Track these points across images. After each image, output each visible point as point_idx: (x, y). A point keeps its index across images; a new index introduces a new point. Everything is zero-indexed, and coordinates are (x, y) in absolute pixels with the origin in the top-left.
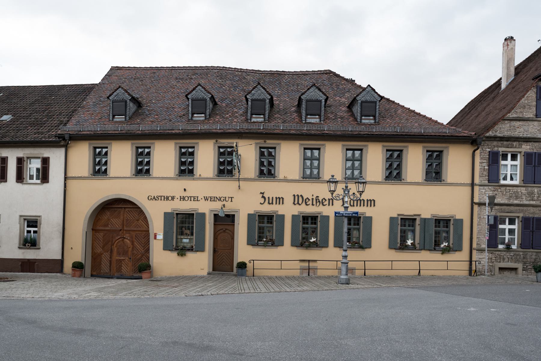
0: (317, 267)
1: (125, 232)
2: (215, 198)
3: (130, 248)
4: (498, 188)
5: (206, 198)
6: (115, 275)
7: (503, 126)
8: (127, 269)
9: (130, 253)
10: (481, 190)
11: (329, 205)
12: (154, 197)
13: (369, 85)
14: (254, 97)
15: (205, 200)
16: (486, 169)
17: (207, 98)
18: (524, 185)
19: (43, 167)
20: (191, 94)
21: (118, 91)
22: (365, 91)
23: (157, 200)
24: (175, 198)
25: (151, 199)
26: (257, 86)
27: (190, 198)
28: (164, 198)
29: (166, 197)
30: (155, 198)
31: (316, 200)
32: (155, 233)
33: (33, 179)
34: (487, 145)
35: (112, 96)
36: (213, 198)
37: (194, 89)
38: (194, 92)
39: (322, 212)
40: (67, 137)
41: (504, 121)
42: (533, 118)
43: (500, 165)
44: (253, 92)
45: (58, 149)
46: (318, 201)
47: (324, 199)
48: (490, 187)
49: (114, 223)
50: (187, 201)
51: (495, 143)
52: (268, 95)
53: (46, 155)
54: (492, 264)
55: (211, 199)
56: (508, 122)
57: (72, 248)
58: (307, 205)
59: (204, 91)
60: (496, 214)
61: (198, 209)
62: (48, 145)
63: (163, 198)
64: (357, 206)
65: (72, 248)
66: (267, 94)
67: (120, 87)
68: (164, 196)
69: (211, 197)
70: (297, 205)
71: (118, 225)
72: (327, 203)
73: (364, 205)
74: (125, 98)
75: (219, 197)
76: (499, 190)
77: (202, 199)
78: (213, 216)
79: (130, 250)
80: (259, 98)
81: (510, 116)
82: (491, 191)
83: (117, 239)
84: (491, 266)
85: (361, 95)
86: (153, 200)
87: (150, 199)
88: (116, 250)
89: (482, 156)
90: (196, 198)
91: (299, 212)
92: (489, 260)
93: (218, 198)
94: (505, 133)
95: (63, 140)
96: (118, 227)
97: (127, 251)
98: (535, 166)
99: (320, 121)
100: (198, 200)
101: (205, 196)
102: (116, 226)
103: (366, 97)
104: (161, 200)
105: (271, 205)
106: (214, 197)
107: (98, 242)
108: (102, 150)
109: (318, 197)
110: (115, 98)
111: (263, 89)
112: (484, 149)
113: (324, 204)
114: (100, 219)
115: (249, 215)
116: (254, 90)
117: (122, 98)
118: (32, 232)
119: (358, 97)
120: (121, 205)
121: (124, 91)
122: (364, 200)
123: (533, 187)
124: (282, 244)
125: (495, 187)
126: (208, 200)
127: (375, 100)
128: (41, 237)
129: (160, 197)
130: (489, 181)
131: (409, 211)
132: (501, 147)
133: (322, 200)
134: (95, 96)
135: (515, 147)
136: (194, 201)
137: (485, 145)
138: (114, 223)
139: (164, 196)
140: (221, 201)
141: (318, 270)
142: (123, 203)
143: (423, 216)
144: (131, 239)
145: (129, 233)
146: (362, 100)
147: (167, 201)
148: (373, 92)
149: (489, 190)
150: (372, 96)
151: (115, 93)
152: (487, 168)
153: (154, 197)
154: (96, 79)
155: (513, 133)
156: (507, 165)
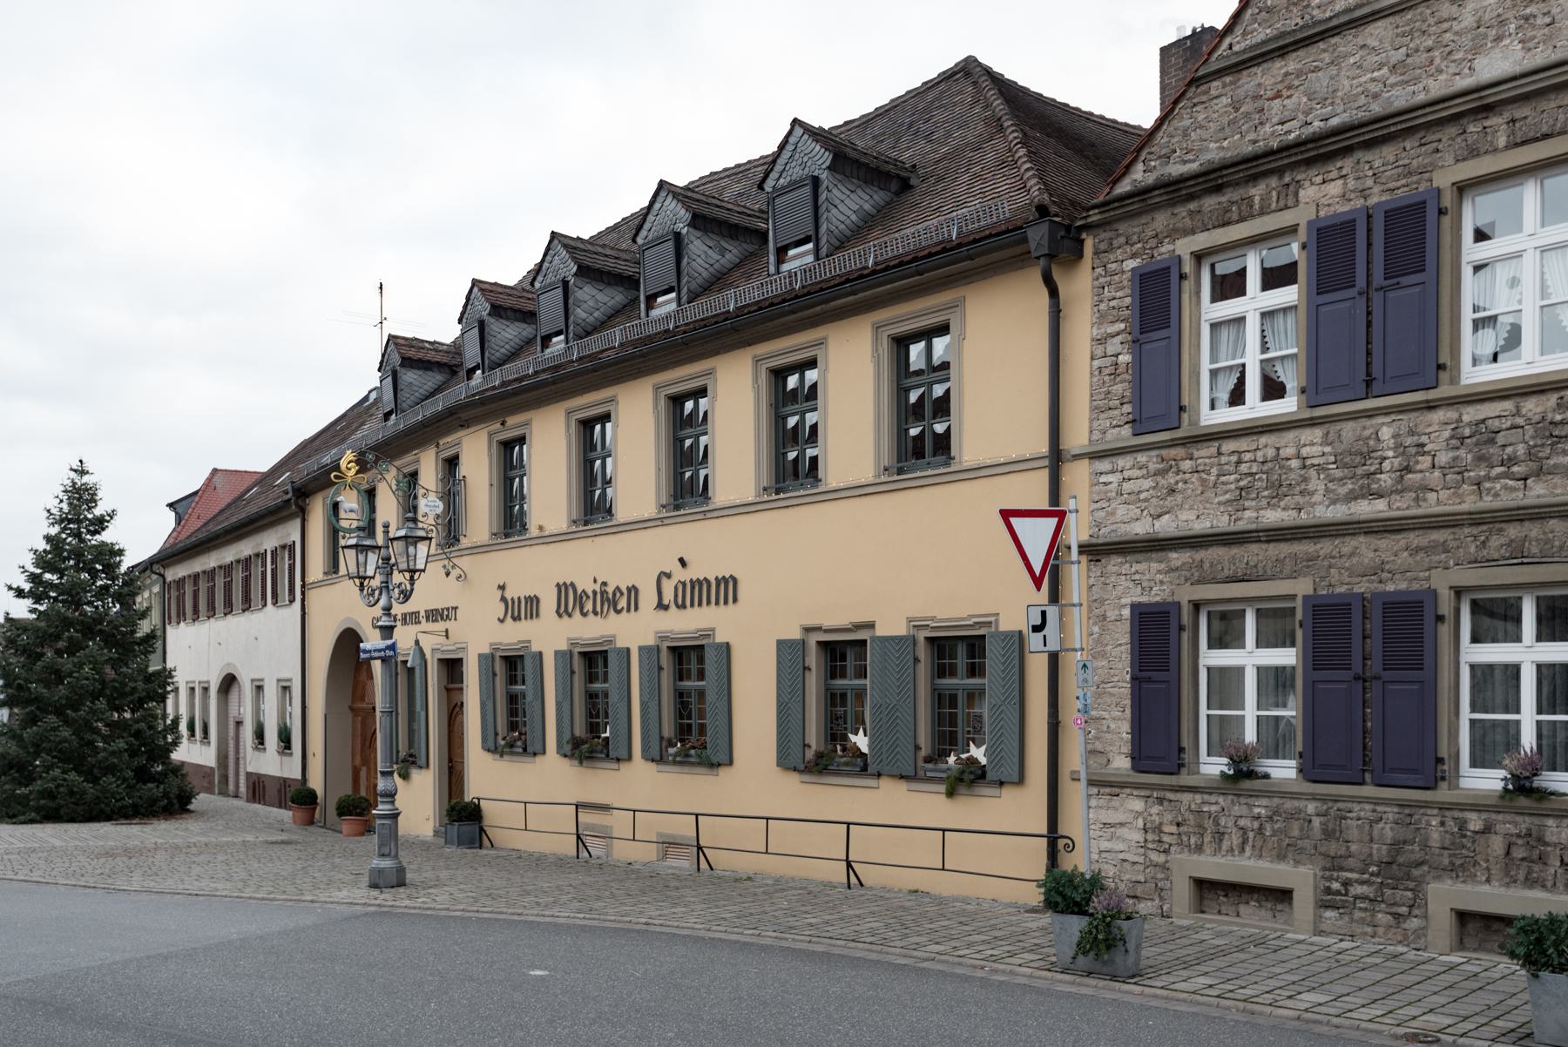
10: (1103, 479)
11: (628, 610)
48: (1142, 458)
51: (1161, 220)
61: (529, 642)
72: (623, 603)
76: (1187, 465)
89: (1103, 306)
92: (1150, 837)
112: (1114, 266)
125: (1164, 452)
155: (1252, 136)
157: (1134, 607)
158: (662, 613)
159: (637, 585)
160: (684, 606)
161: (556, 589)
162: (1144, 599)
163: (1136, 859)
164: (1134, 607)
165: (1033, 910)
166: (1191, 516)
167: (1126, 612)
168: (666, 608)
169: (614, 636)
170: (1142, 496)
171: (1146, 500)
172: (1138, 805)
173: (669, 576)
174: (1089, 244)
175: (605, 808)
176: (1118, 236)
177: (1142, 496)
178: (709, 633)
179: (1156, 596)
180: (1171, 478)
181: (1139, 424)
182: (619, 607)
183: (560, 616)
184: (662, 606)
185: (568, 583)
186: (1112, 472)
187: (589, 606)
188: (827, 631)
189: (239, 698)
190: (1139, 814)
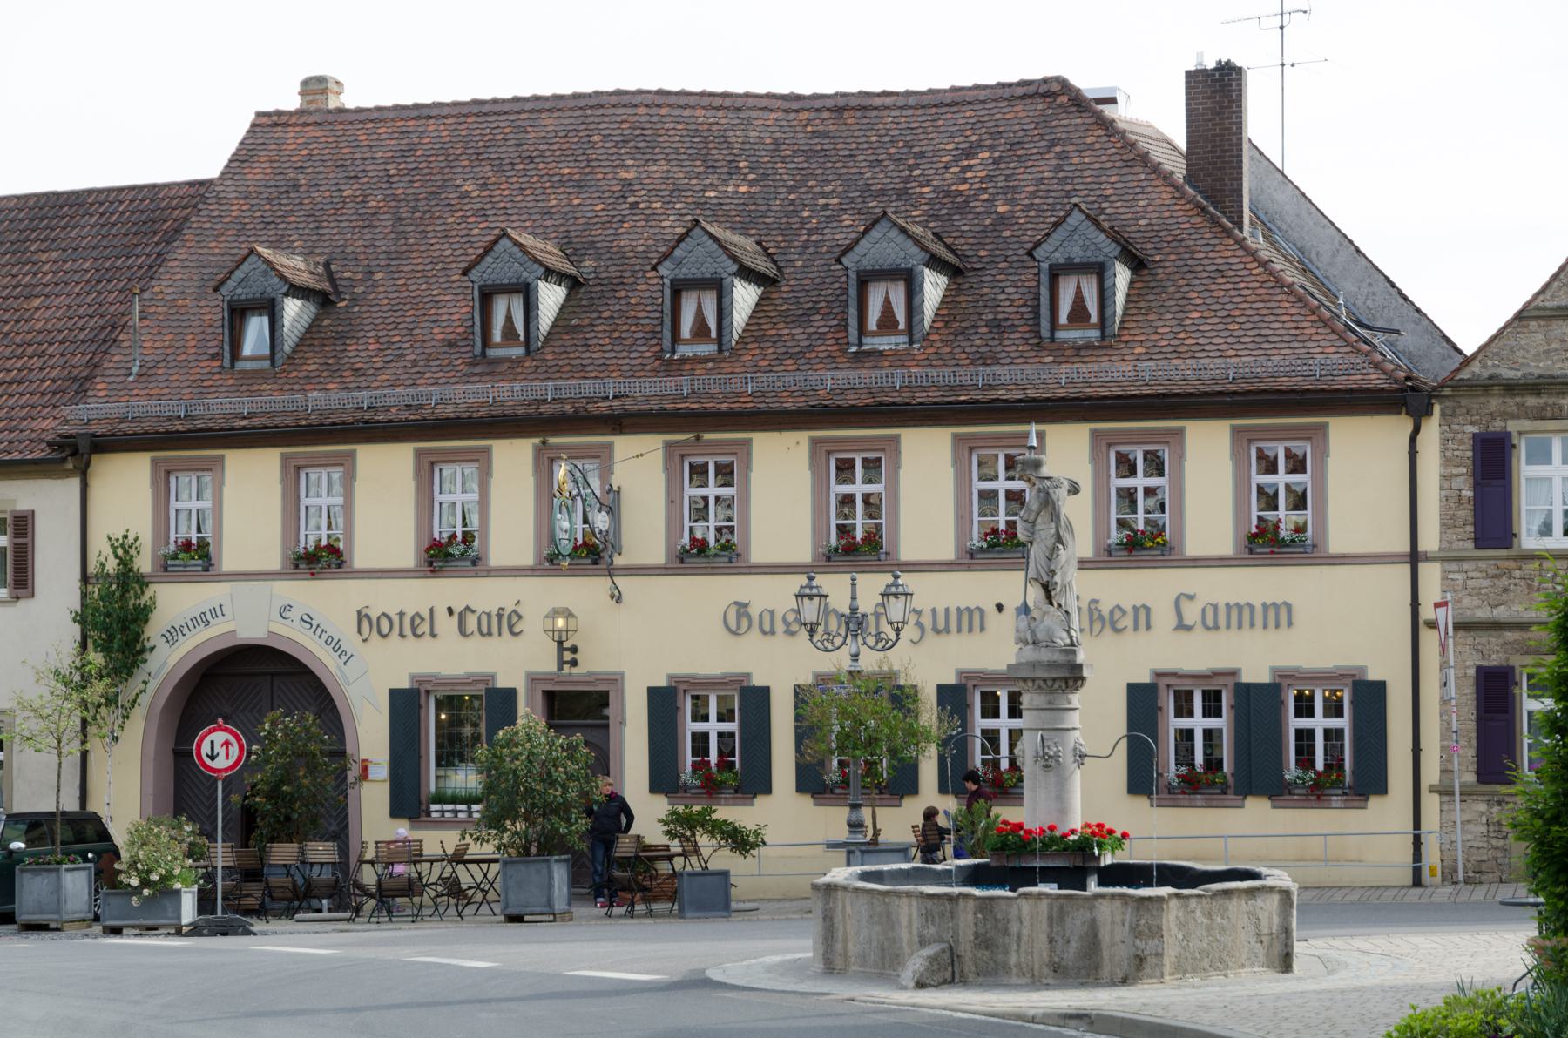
4: (1512, 564)
7: (1523, 342)
10: (1451, 576)
11: (1136, 628)
14: (683, 273)
16: (1464, 500)
17: (530, 280)
20: (478, 268)
21: (246, 264)
22: (1064, 225)
26: (690, 230)
32: (363, 761)
34: (1464, 411)
35: (229, 282)
37: (488, 249)
38: (489, 259)
40: (83, 445)
41: (1525, 323)
43: (1523, 482)
44: (677, 252)
45: (59, 481)
46: (1096, 615)
47: (1118, 607)
48: (1483, 565)
51: (1494, 403)
52: (730, 262)
53: (23, 506)
54: (1501, 843)
56: (1540, 326)
58: (1118, 631)
59: (520, 254)
60: (1507, 659)
64: (959, 631)
66: (724, 257)
72: (1127, 622)
73: (1252, 625)
74: (269, 290)
76: (1517, 573)
78: (539, 697)
80: (699, 276)
81: (1548, 304)
82: (1487, 577)
84: (1497, 848)
85: (1050, 240)
89: (1448, 454)
92: (1491, 828)
94: (1528, 365)
95: (73, 455)
103: (1069, 249)
105: (1269, 602)
109: (1095, 601)
110: (239, 291)
111: (711, 241)
112: (1457, 427)
113: (1120, 626)
115: (394, 694)
116: (682, 245)
117: (260, 290)
119: (1039, 250)
121: (264, 266)
122: (1252, 607)
124: (767, 789)
125: (1500, 563)
127: (1100, 259)
132: (1518, 417)
133: (1112, 612)
134: (187, 264)
137: (1458, 412)
143: (1246, 678)
146: (1054, 261)
148: (1093, 228)
149: (1479, 575)
150: (1087, 243)
151: (238, 274)
152: (1468, 493)
154: (208, 162)
155: (1560, 365)
156: (1550, 479)
157: (1479, 669)
158: (1183, 635)
159: (1289, 601)
160: (490, 634)
162: (1484, 663)
163: (1481, 845)
164: (1479, 669)
165: (1409, 887)
166: (1521, 608)
167: (1472, 672)
168: (1189, 628)
170: (1483, 591)
171: (1486, 594)
172: (1482, 807)
173: (1191, 597)
174: (1437, 409)
176: (1460, 407)
177: (1483, 591)
179: (1495, 660)
180: (1504, 581)
181: (1481, 542)
182: (419, 632)
184: (1182, 626)
186: (1459, 572)
190: (1482, 813)
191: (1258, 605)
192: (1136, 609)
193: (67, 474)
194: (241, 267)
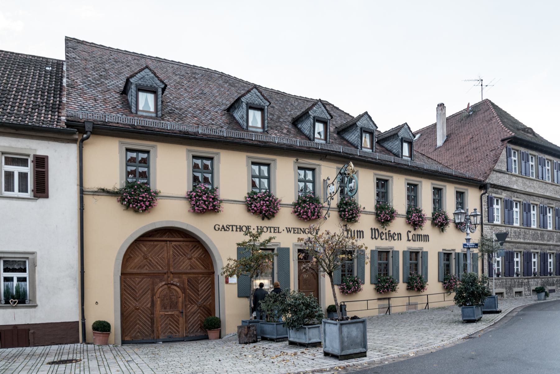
0: (417, 302)
1: (171, 275)
2: (299, 229)
3: (180, 298)
5: (288, 230)
6: (161, 338)
8: (177, 328)
9: (180, 305)
11: (398, 240)
12: (223, 226)
13: (406, 123)
15: (288, 232)
18: (505, 225)
19: (37, 171)
23: (227, 230)
24: (250, 229)
25: (219, 229)
27: (269, 229)
28: (237, 228)
29: (238, 227)
30: (224, 228)
31: (389, 234)
33: (13, 191)
36: (297, 230)
39: (393, 247)
40: (89, 127)
42: (505, 171)
45: (63, 144)
48: (489, 226)
49: (155, 263)
50: (267, 232)
53: (41, 152)
55: (294, 230)
57: (97, 302)
61: (280, 243)
62: (49, 137)
63: (234, 228)
64: (417, 241)
65: (97, 302)
67: (147, 67)
68: (236, 226)
69: (294, 228)
70: (374, 239)
71: (160, 266)
74: (155, 85)
75: (304, 229)
77: (283, 230)
79: (180, 301)
83: (161, 285)
86: (221, 230)
87: (217, 229)
88: (159, 302)
90: (277, 229)
91: (376, 247)
93: (303, 230)
96: (161, 269)
97: (177, 303)
98: (509, 210)
99: (373, 151)
100: (280, 232)
101: (288, 227)
102: (157, 267)
104: (232, 230)
106: (298, 229)
107: (130, 291)
108: (137, 155)
110: (140, 82)
114: (131, 257)
118: (15, 280)
120: (166, 237)
123: (508, 227)
126: (291, 232)
128: (37, 287)
129: (231, 227)
130: (488, 220)
131: (449, 248)
135: (499, 194)
136: (294, 234)
138: (155, 263)
139: (236, 226)
140: (306, 233)
141: (378, 308)
142: (168, 233)
144: (182, 286)
145: (179, 278)
147: (240, 232)
151: (139, 75)
153: (223, 226)
159: (363, 231)
160: (415, 241)
161: (370, 231)
169: (393, 247)
173: (410, 232)
175: (379, 299)
178: (421, 249)
183: (372, 238)
185: (376, 229)
187: (384, 237)
188: (381, 249)
189: (448, 267)
191: (423, 235)
192: (398, 234)
193: (74, 141)
194: (141, 73)
